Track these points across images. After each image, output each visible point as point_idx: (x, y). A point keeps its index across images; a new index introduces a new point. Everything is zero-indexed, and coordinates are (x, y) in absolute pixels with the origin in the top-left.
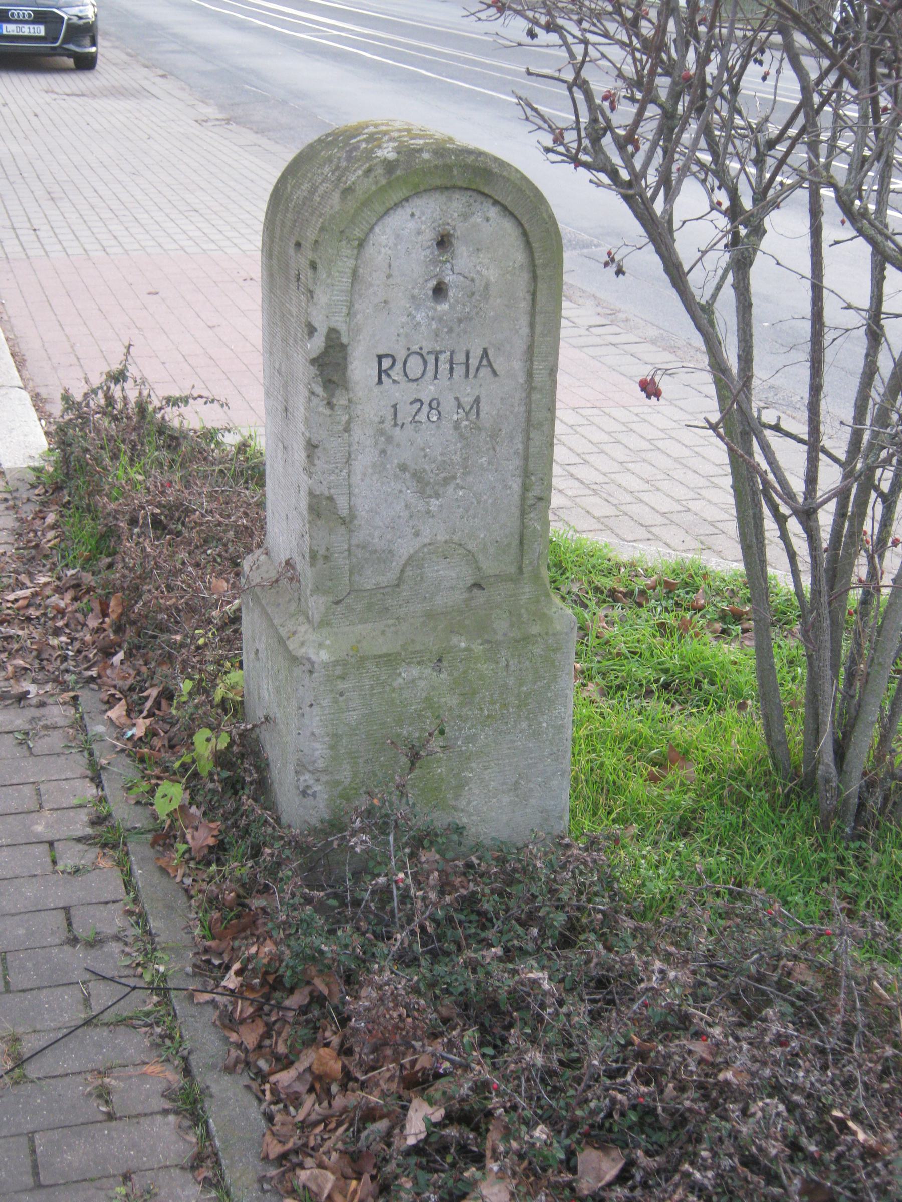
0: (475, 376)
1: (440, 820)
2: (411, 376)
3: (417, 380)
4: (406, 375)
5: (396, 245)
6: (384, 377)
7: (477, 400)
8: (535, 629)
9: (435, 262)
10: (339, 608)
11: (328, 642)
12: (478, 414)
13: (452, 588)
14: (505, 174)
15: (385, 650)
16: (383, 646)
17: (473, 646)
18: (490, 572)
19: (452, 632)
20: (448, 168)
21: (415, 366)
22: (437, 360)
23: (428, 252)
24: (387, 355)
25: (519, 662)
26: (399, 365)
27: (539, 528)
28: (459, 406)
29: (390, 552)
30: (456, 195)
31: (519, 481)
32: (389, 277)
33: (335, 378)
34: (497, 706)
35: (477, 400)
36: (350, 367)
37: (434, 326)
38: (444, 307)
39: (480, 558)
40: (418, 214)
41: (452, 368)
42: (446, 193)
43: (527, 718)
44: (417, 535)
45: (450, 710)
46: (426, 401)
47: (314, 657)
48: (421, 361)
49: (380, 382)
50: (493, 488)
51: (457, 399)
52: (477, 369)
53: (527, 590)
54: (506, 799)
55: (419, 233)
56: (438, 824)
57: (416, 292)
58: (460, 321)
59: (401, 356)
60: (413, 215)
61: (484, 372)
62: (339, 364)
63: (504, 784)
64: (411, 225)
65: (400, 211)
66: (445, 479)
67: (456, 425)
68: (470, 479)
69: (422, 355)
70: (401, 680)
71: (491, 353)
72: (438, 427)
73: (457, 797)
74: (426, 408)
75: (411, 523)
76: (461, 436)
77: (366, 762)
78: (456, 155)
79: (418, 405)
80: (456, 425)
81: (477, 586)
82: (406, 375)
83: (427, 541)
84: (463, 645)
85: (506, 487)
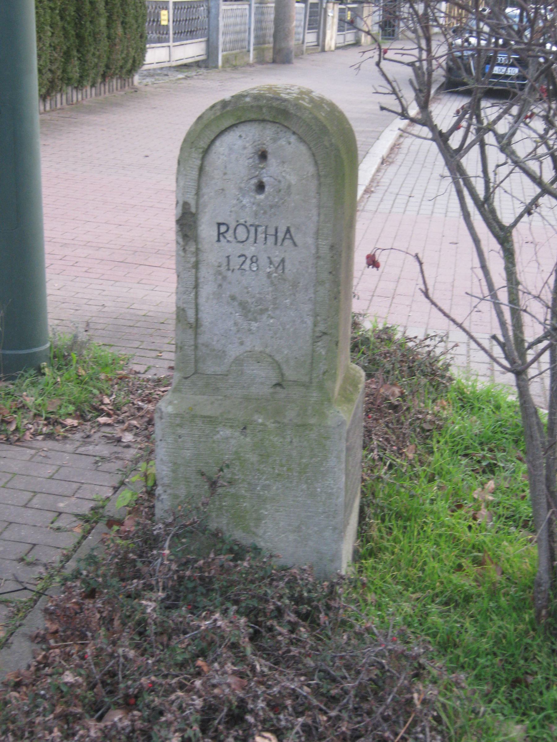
0: (282, 245)
1: (246, 540)
2: (239, 239)
3: (243, 242)
4: (236, 238)
5: (230, 154)
6: (222, 238)
7: (283, 261)
8: (313, 421)
9: (255, 167)
10: (188, 382)
11: (176, 402)
12: (283, 269)
13: (262, 383)
14: (299, 114)
15: (209, 414)
16: (208, 411)
17: (268, 423)
18: (292, 378)
19: (257, 411)
20: (260, 108)
21: (242, 233)
22: (256, 231)
23: (251, 160)
24: (223, 224)
25: (300, 441)
26: (231, 231)
27: (323, 353)
28: (271, 263)
29: (224, 352)
30: (269, 126)
31: (312, 319)
32: (225, 174)
33: (189, 234)
34: (285, 468)
35: (283, 261)
36: (200, 228)
37: (254, 208)
38: (262, 197)
39: (284, 367)
40: (244, 136)
41: (266, 238)
42: (262, 124)
43: (306, 483)
44: (242, 343)
45: (252, 464)
46: (249, 256)
47: (163, 409)
48: (245, 230)
49: (219, 240)
50: (294, 321)
51: (269, 258)
52: (283, 240)
53: (315, 395)
54: (291, 537)
55: (245, 148)
56: (228, 534)
57: (243, 185)
58: (271, 207)
59: (233, 225)
60: (240, 136)
61: (287, 242)
62: (191, 225)
63: (289, 525)
64: (240, 143)
65: (232, 133)
66: (261, 310)
67: (269, 275)
68: (278, 312)
69: (246, 227)
70: (218, 436)
71: (292, 230)
72: (257, 275)
73: (257, 526)
74: (248, 262)
75: (239, 335)
76: (272, 283)
77: (196, 486)
78: (268, 100)
79: (243, 259)
80: (269, 275)
81: (278, 385)
82: (236, 238)
83: (248, 349)
84: (260, 421)
85: (303, 322)
